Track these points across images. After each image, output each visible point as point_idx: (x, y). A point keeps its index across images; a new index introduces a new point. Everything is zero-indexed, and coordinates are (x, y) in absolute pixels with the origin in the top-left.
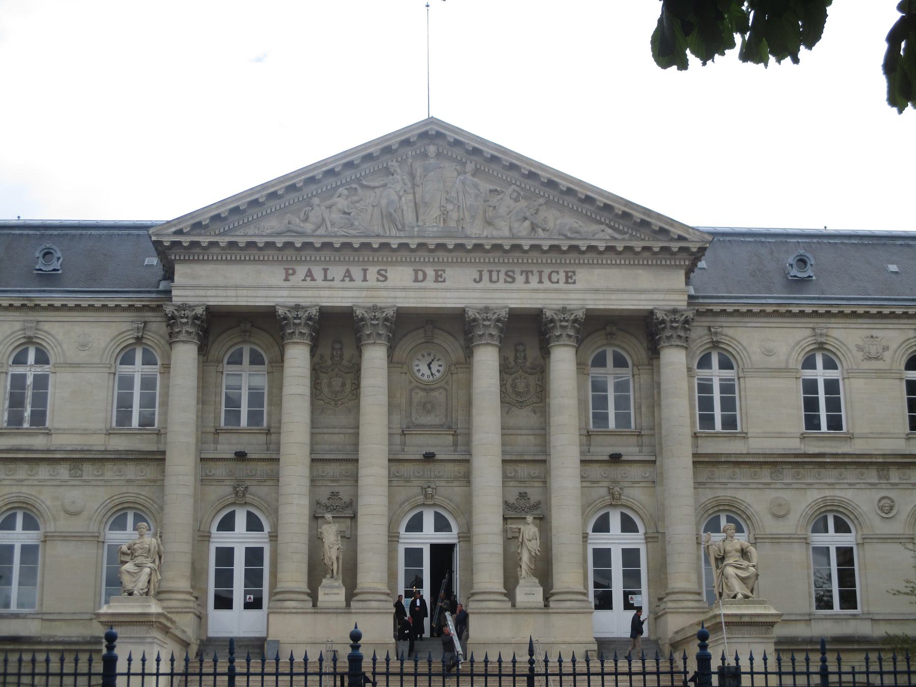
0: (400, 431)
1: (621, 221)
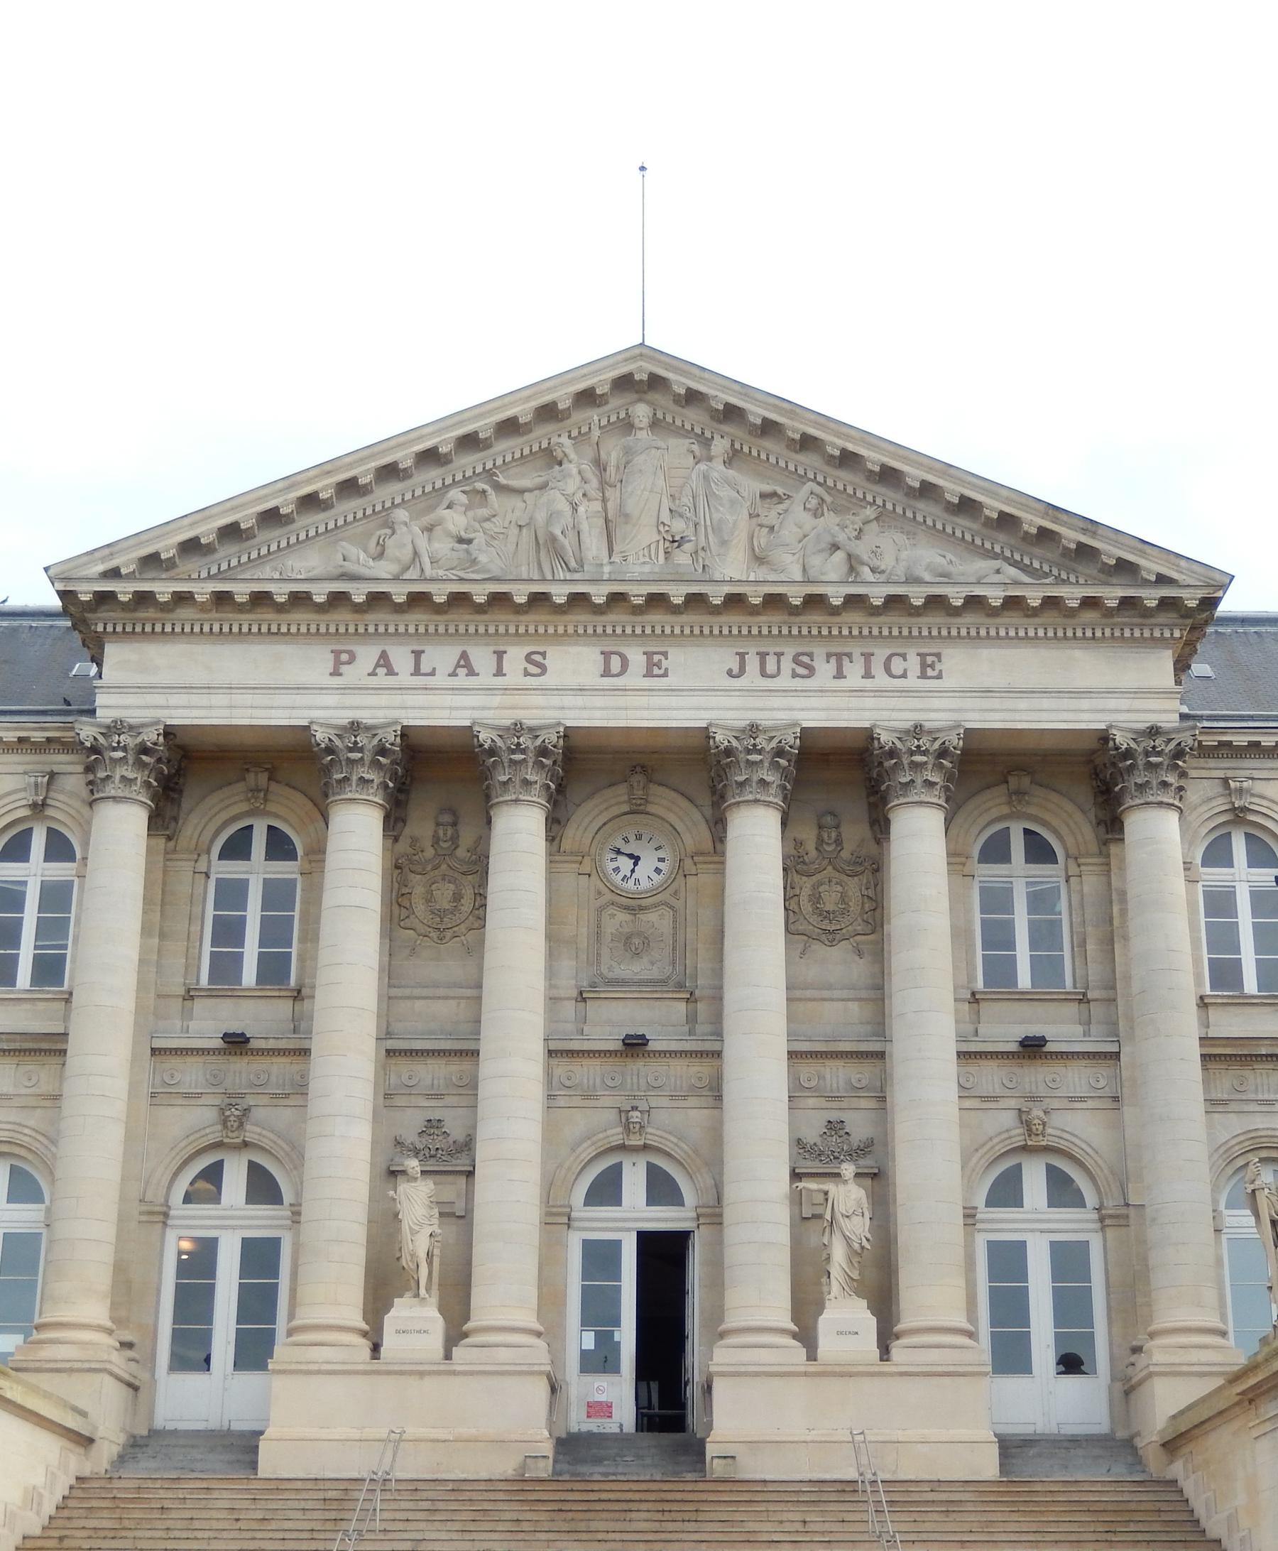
0: (575, 993)
1: (1037, 551)
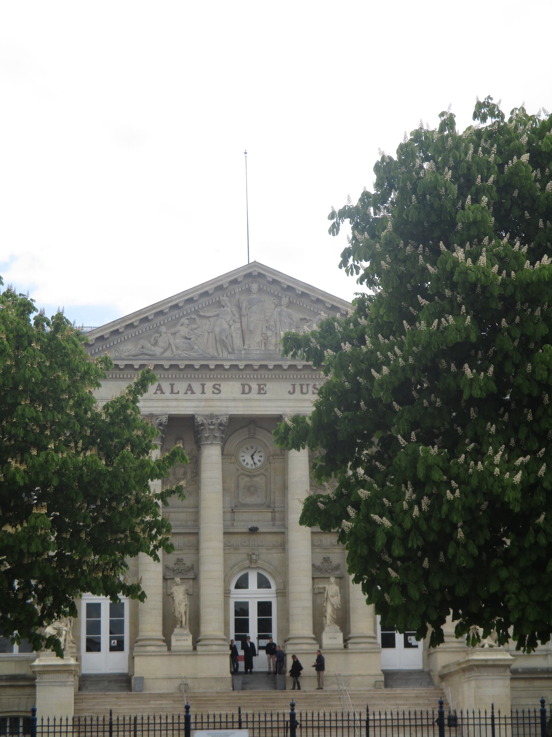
0: (230, 510)
